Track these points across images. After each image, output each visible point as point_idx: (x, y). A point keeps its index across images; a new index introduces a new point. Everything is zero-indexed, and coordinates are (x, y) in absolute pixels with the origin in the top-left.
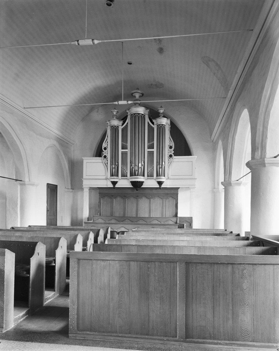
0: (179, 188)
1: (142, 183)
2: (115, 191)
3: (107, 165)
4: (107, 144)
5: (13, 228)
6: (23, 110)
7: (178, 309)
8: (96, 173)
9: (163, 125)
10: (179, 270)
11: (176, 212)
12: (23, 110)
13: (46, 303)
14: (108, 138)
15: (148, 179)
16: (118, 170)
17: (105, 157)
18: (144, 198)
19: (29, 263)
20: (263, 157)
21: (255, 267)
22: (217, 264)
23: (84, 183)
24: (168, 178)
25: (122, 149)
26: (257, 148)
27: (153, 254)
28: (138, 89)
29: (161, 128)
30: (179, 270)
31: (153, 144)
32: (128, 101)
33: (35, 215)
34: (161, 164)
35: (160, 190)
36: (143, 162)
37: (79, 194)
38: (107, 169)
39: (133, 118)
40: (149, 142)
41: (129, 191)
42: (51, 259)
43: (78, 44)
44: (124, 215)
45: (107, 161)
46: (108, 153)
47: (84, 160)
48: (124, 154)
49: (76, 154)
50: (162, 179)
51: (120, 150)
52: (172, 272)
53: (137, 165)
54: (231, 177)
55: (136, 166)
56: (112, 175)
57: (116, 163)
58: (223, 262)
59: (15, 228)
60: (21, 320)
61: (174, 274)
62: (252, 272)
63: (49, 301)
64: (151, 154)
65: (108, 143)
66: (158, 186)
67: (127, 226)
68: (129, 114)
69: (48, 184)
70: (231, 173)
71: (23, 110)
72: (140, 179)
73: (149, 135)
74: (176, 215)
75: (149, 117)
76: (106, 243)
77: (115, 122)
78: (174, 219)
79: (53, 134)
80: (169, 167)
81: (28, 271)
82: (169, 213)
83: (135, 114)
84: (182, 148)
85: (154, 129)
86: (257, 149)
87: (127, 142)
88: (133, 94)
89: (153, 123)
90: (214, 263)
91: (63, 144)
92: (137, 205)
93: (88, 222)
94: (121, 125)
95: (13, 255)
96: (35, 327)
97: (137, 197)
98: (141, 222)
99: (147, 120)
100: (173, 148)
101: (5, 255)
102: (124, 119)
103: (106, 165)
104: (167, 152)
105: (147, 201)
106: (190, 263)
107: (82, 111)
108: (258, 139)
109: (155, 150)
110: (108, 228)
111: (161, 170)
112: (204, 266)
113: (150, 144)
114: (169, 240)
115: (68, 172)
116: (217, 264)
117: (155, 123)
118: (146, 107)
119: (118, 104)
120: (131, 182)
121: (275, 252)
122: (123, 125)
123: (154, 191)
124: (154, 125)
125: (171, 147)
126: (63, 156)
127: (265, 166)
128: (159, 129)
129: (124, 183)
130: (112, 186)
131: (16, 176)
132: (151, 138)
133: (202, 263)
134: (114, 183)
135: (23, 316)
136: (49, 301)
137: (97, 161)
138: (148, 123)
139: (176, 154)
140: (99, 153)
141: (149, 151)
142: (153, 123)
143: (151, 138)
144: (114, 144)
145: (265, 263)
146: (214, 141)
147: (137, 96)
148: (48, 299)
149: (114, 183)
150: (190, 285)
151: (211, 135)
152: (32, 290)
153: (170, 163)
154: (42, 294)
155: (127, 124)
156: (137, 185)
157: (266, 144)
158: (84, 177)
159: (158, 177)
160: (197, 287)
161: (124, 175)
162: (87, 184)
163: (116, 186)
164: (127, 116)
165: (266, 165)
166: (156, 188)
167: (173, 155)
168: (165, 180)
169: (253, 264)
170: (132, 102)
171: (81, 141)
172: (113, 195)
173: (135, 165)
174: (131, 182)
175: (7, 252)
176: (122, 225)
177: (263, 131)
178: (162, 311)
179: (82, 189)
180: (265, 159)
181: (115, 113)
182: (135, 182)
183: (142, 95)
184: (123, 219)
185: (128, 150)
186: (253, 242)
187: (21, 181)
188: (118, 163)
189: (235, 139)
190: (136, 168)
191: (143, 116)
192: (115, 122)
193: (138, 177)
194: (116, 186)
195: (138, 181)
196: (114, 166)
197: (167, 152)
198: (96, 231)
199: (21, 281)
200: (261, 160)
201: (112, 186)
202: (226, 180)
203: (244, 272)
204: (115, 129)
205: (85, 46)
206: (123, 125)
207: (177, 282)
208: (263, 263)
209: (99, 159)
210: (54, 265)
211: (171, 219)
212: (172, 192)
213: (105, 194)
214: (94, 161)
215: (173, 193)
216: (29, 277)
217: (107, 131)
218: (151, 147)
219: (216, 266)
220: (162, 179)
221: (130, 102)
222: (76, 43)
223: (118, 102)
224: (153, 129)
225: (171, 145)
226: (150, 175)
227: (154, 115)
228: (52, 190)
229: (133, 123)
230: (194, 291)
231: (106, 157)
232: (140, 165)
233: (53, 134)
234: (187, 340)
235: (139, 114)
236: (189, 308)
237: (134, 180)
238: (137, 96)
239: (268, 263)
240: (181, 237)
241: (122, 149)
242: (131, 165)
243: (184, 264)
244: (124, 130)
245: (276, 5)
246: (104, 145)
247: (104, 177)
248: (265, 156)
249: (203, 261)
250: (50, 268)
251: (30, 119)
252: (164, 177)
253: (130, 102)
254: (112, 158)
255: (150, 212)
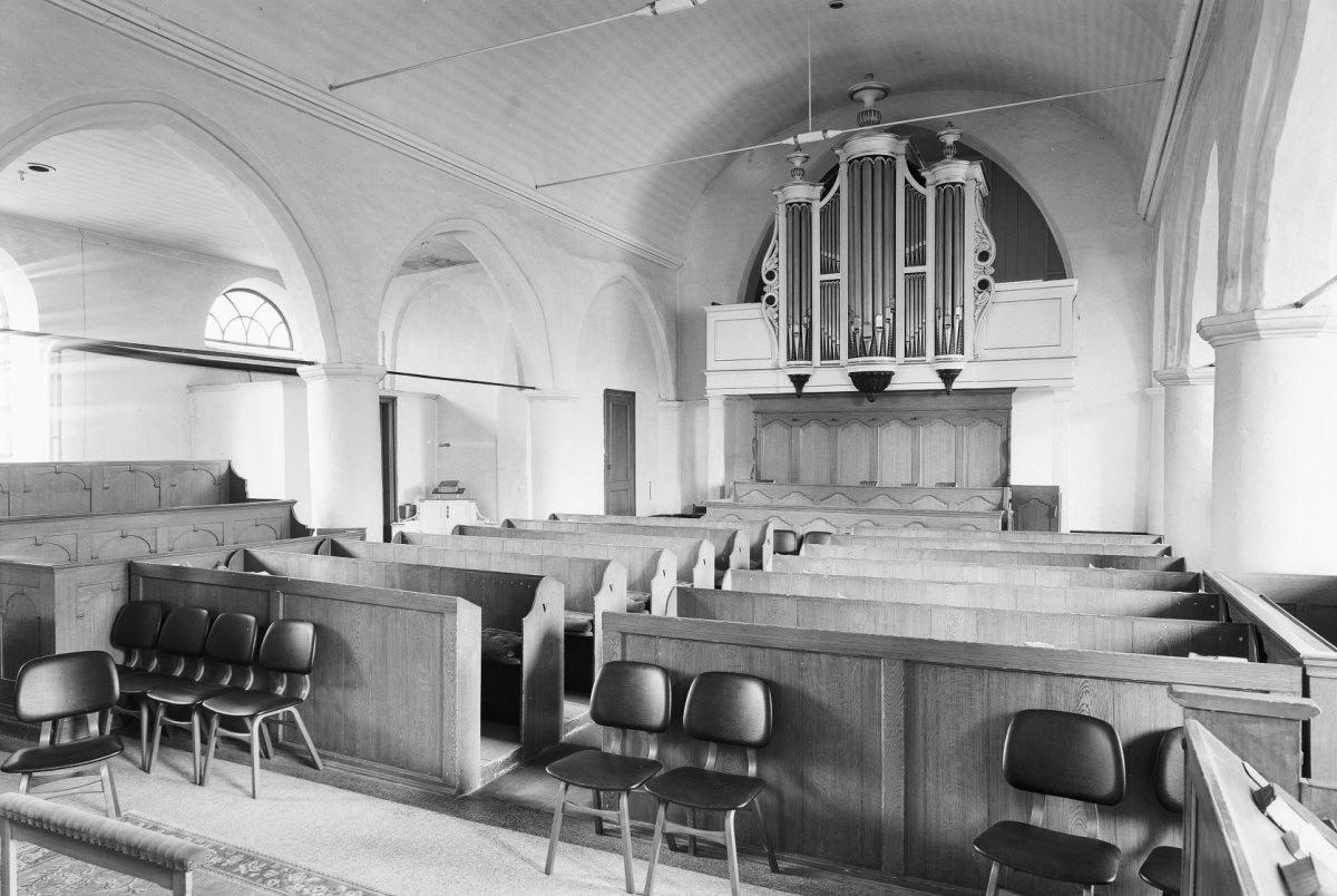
0: (1015, 388)
1: (887, 377)
2: (803, 404)
3: (776, 325)
4: (777, 261)
5: (509, 524)
6: (535, 193)
7: (883, 791)
8: (747, 350)
9: (954, 184)
10: (887, 681)
11: (1004, 468)
12: (535, 194)
13: (566, 736)
14: (781, 244)
15: (906, 363)
16: (811, 335)
17: (771, 300)
18: (895, 426)
19: (519, 630)
20: (1251, 304)
21: (1120, 687)
22: (999, 670)
24: (976, 359)
25: (823, 271)
26: (1229, 276)
27: (812, 631)
28: (871, 76)
29: (951, 196)
30: (886, 682)
31: (924, 247)
32: (825, 131)
33: (577, 487)
34: (950, 313)
35: (946, 397)
36: (888, 310)
37: (699, 412)
38: (778, 337)
39: (857, 171)
40: (908, 243)
41: (848, 404)
42: (581, 618)
43: (655, 13)
44: (831, 479)
45: (778, 312)
46: (778, 288)
47: (709, 315)
48: (830, 289)
49: (689, 294)
50: (954, 362)
51: (817, 277)
52: (866, 684)
53: (870, 320)
54: (1188, 353)
55: (868, 323)
56: (792, 356)
57: (805, 320)
58: (1015, 667)
59: (514, 523)
60: (503, 771)
61: (873, 693)
62: (1110, 705)
63: (576, 730)
64: (916, 282)
65: (777, 256)
66: (942, 386)
67: (834, 517)
68: (843, 159)
69: (608, 392)
70: (1189, 339)
71: (535, 194)
72: (880, 364)
74: (1004, 481)
75: (908, 162)
76: (727, 585)
77: (800, 192)
78: (994, 496)
79: (618, 243)
80: (976, 322)
81: (518, 650)
82: (978, 470)
83: (860, 159)
84: (1029, 249)
86: (1233, 277)
87: (836, 249)
88: (855, 97)
89: (922, 181)
90: (989, 669)
91: (651, 269)
92: (874, 448)
93: (723, 500)
94: (819, 196)
95: (477, 611)
96: (528, 790)
97: (872, 421)
98: (883, 503)
99: (903, 172)
100: (991, 260)
101: (456, 612)
102: (828, 180)
103: (774, 324)
105: (906, 432)
106: (919, 662)
107: (704, 170)
108: (1236, 244)
109: (929, 268)
110: (767, 525)
111: (948, 332)
112: (958, 674)
114: (911, 580)
115: (666, 348)
116: (999, 670)
117: (928, 181)
118: (898, 131)
119: (796, 142)
120: (851, 375)
121: (1241, 639)
122: (824, 195)
123: (930, 402)
125: (984, 256)
126: (651, 306)
127: (1257, 337)
128: (942, 199)
129: (830, 379)
130: (793, 390)
131: (521, 377)
132: (916, 231)
133: (952, 666)
134: (800, 381)
135: (506, 763)
136: (576, 730)
137: (747, 314)
138: (906, 182)
140: (754, 291)
142: (922, 181)
143: (916, 231)
144: (797, 260)
145: (1151, 678)
146: (1149, 219)
147: (868, 99)
148: (572, 725)
149: (800, 381)
150: (919, 726)
151: (1137, 200)
152: (528, 702)
153: (981, 309)
154: (556, 709)
155: (838, 191)
156: (872, 385)
157: (1261, 258)
158: (711, 365)
159: (938, 357)
160: (938, 733)
161: (829, 355)
162: (719, 384)
163: (806, 389)
164: (837, 166)
165: (1261, 332)
166: (936, 393)
167: (991, 280)
169: (1110, 679)
170: (840, 132)
171: (708, 257)
172: (795, 417)
173: (863, 320)
174: (852, 375)
175: (462, 603)
176: (817, 514)
177: (1251, 219)
178: (838, 790)
179: (702, 398)
180: (1257, 314)
181: (798, 163)
182: (863, 373)
183: (886, 92)
184: (828, 490)
185: (842, 276)
186: (1185, 601)
187: (533, 388)
188: (811, 317)
189: (1197, 224)
190: (868, 332)
191: (889, 163)
192: (800, 192)
193: (874, 358)
194: (806, 389)
195: (872, 373)
196: (797, 329)
197: (972, 271)
198: (729, 535)
199: (499, 672)
200: (1242, 317)
201: (793, 390)
202: (1169, 365)
203: (1082, 701)
204: (799, 213)
205: (673, 13)
206: (824, 195)
207: (880, 715)
208: (1144, 678)
209: (754, 309)
210: (591, 634)
211: (986, 494)
212: (992, 401)
213: (793, 409)
214: (739, 315)
215: (994, 406)
216: (521, 666)
217: (773, 224)
218: (917, 258)
219: (995, 676)
220: (954, 362)
221: (831, 134)
222: (647, 11)
223: (795, 137)
224: (923, 200)
225: (986, 248)
226: (915, 351)
227: (925, 149)
228: (620, 407)
229: (857, 189)
230: (929, 744)
232: (879, 320)
233: (618, 243)
234: (909, 879)
235: (874, 157)
236: (916, 791)
237: (859, 370)
238: (868, 99)
239: (1160, 680)
240: (965, 569)
241: (823, 271)
242: (851, 323)
243: (899, 664)
244: (830, 213)
245: (13, 890)
246: (767, 265)
247: (768, 364)
248: (1259, 301)
249: (956, 661)
250: (578, 642)
251: (555, 215)
252: (960, 356)
253: (831, 134)
254: (790, 302)
255: (915, 468)
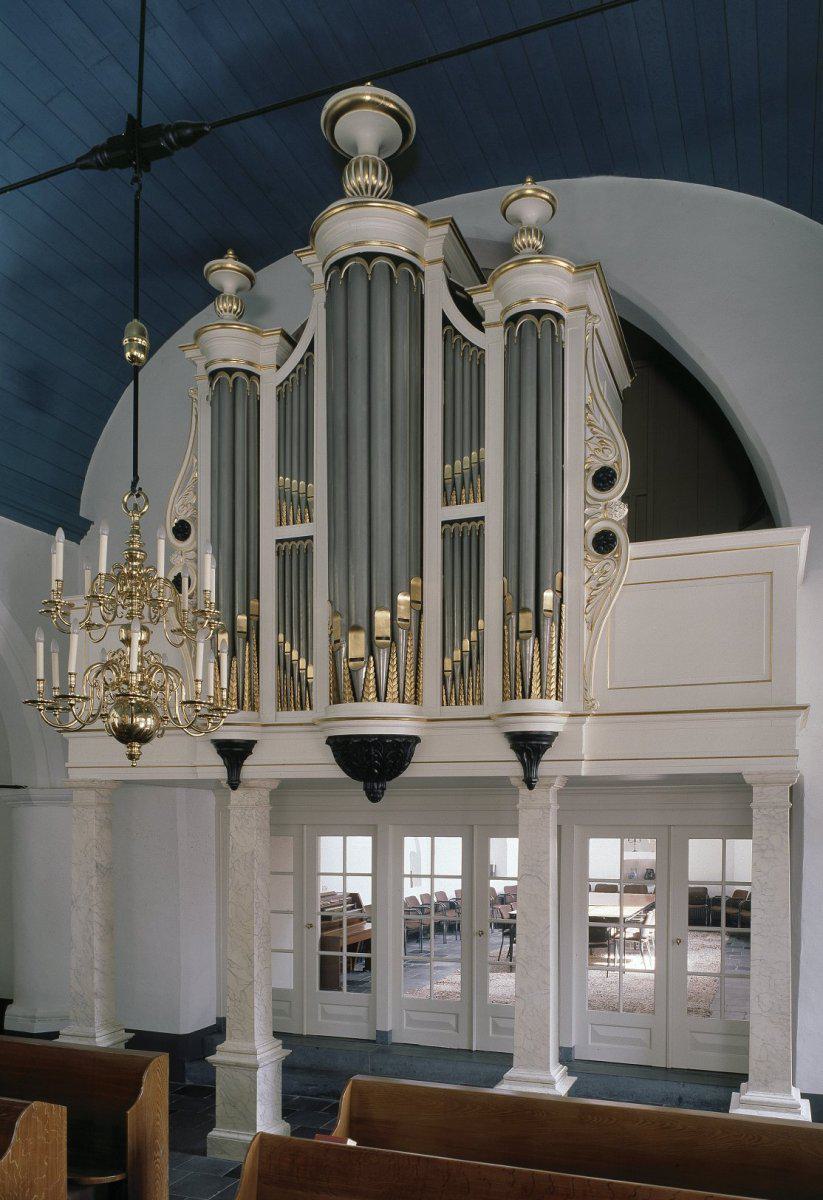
23: (491, 983)
29: (534, 331)
40: (449, 455)
48: (296, 555)
72: (386, 718)
73: (449, 383)
85: (483, 356)
89: (475, 317)
94: (274, 361)
99: (438, 301)
100: (622, 484)
104: (586, 511)
113: (466, 458)
124: (482, 329)
125: (604, 479)
138: (446, 321)
139: (642, 528)
141: (451, 522)
142: (475, 317)
153: (601, 586)
155: (311, 348)
161: (294, 693)
167: (622, 535)
168: (565, 720)
185: (316, 528)
197: (586, 511)
220: (546, 715)
224: (479, 357)
231: (177, 537)
252: (551, 704)
